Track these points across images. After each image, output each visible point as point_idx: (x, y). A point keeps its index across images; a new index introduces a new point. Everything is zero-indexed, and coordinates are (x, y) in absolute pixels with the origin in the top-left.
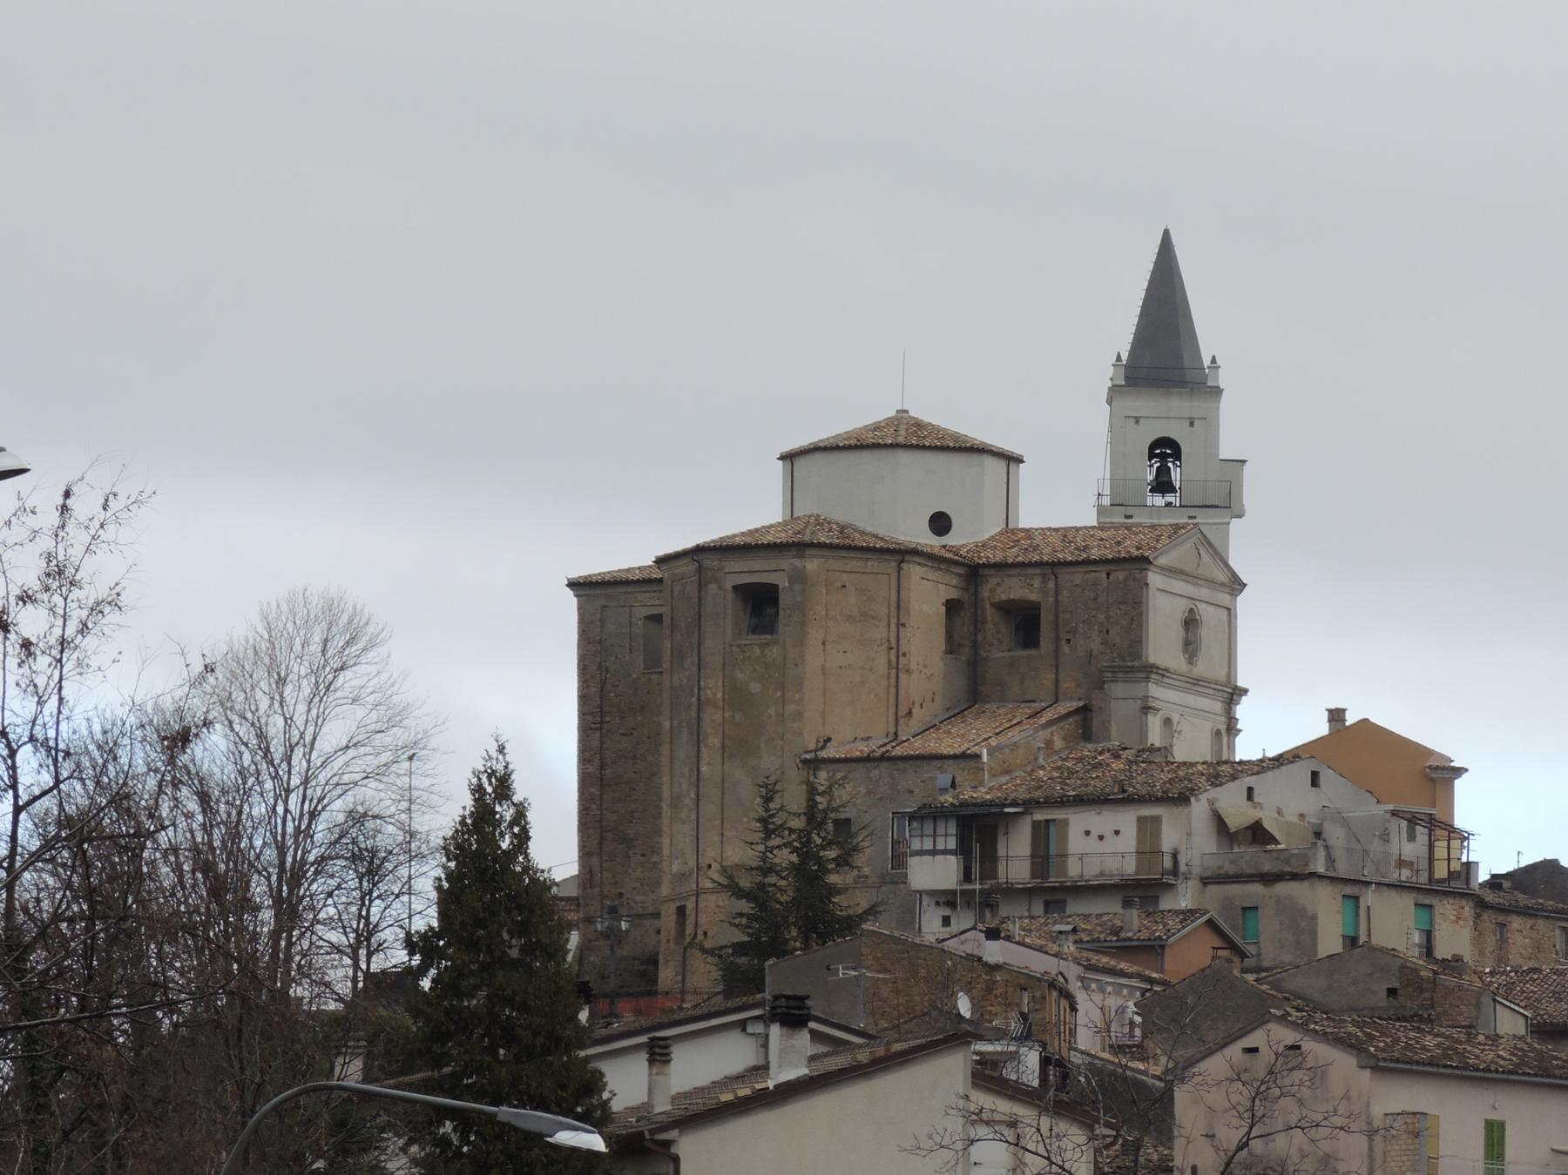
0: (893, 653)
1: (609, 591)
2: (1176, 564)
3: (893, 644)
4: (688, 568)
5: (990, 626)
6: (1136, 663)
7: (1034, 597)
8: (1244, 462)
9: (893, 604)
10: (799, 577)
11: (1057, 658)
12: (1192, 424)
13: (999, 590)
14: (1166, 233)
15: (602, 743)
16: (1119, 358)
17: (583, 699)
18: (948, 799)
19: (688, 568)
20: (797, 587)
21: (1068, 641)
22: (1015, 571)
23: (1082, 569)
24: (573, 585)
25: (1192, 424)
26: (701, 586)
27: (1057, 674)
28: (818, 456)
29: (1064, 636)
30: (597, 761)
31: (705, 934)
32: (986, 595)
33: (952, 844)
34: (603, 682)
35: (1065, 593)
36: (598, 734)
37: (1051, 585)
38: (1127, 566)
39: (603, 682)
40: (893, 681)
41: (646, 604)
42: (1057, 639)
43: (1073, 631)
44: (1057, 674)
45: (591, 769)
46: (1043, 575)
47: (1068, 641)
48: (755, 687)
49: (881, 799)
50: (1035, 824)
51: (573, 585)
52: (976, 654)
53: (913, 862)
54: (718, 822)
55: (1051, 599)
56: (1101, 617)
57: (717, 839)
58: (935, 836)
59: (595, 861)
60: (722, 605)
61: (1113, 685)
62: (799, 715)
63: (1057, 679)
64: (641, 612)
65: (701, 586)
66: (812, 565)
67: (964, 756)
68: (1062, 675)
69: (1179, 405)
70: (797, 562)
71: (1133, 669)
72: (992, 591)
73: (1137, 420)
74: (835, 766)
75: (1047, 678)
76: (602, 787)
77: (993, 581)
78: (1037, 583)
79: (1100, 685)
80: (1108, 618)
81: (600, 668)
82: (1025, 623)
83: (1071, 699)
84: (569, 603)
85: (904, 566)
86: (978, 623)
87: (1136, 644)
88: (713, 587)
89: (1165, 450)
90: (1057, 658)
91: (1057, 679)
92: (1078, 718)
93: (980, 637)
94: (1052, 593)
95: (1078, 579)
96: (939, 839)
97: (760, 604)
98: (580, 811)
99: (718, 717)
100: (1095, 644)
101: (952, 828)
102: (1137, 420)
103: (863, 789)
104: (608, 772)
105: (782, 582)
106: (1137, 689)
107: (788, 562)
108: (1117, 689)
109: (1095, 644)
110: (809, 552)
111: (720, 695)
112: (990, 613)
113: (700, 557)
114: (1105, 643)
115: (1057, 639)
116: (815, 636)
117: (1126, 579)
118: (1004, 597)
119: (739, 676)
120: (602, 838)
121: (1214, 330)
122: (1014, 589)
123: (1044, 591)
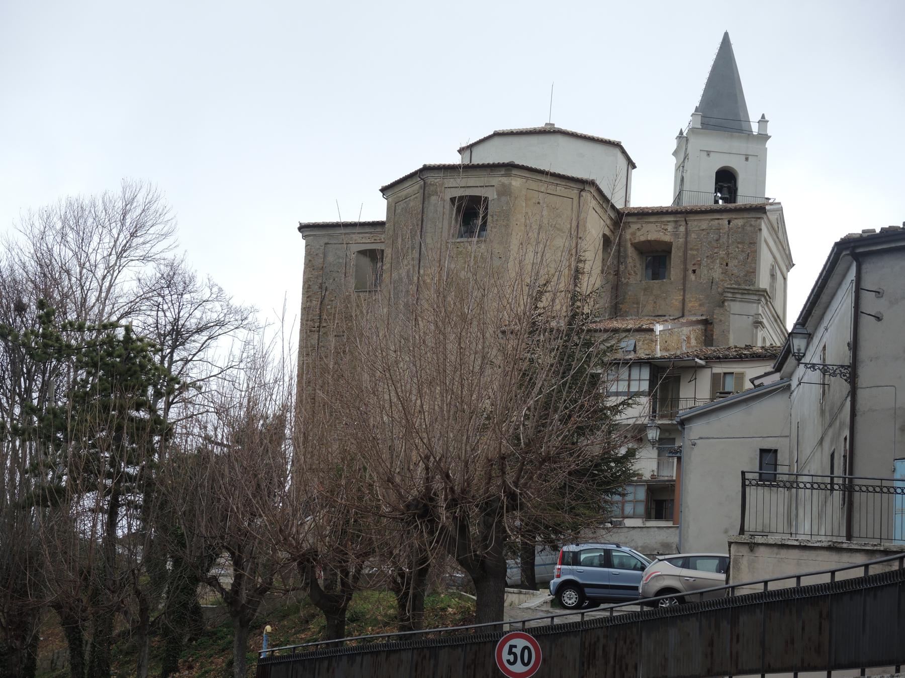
1: (331, 232)
4: (414, 187)
5: (630, 260)
6: (751, 288)
7: (667, 238)
9: (574, 224)
10: (505, 191)
11: (684, 284)
12: (747, 159)
13: (638, 234)
14: (726, 34)
16: (681, 133)
18: (632, 356)
19: (414, 187)
20: (503, 198)
21: (694, 271)
22: (652, 219)
23: (709, 217)
24: (303, 228)
25: (747, 159)
26: (425, 198)
27: (684, 295)
28: (497, 141)
29: (691, 268)
32: (628, 237)
33: (645, 386)
34: (323, 298)
35: (693, 236)
37: (682, 229)
38: (746, 215)
39: (323, 298)
41: (365, 242)
42: (685, 270)
43: (699, 264)
44: (684, 295)
46: (676, 222)
47: (694, 271)
50: (715, 378)
51: (303, 228)
52: (619, 280)
53: (631, 390)
55: (682, 240)
56: (722, 253)
58: (629, 380)
60: (442, 219)
61: (732, 304)
63: (684, 299)
64: (355, 248)
65: (425, 198)
66: (516, 182)
67: (640, 330)
68: (688, 296)
69: (738, 145)
70: (505, 180)
71: (748, 292)
72: (633, 234)
73: (708, 153)
75: (676, 299)
77: (634, 227)
78: (670, 227)
79: (722, 304)
80: (728, 254)
81: (321, 288)
82: (656, 258)
83: (695, 314)
84: (298, 245)
85: (583, 194)
86: (620, 257)
87: (751, 273)
89: (726, 180)
90: (684, 284)
91: (684, 299)
92: (700, 327)
93: (622, 268)
95: (704, 225)
96: (632, 383)
97: (471, 213)
100: (717, 274)
101: (646, 373)
102: (708, 153)
105: (491, 194)
106: (752, 308)
107: (497, 180)
108: (735, 307)
109: (717, 274)
110: (515, 172)
112: (630, 250)
113: (426, 175)
114: (725, 273)
115: (685, 270)
117: (743, 226)
118: (643, 239)
121: (756, 103)
122: (651, 232)
123: (676, 235)
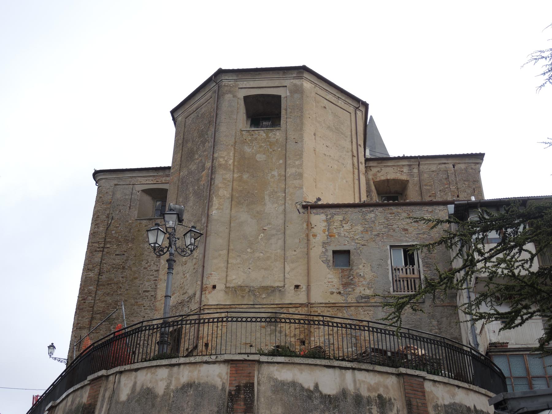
0: (355, 159)
2: (84, 390)
3: (355, 154)
7: (404, 177)
8: (481, 156)
10: (298, 90)
15: (102, 259)
17: (93, 235)
20: (296, 96)
30: (97, 270)
31: (207, 345)
34: (109, 225)
36: (100, 254)
37: (415, 171)
39: (109, 225)
40: (356, 177)
45: (91, 275)
46: (410, 166)
48: (260, 157)
49: (378, 235)
52: (329, 225)
54: (225, 252)
56: (453, 188)
57: (223, 265)
59: (85, 333)
62: (300, 176)
64: (139, 188)
70: (297, 82)
74: (333, 211)
76: (97, 285)
78: (405, 170)
88: (228, 96)
94: (416, 175)
95: (434, 168)
98: (79, 301)
99: (229, 176)
103: (360, 228)
104: (104, 277)
111: (231, 162)
116: (309, 129)
118: (383, 178)
119: (248, 150)
120: (93, 318)
123: (411, 174)
